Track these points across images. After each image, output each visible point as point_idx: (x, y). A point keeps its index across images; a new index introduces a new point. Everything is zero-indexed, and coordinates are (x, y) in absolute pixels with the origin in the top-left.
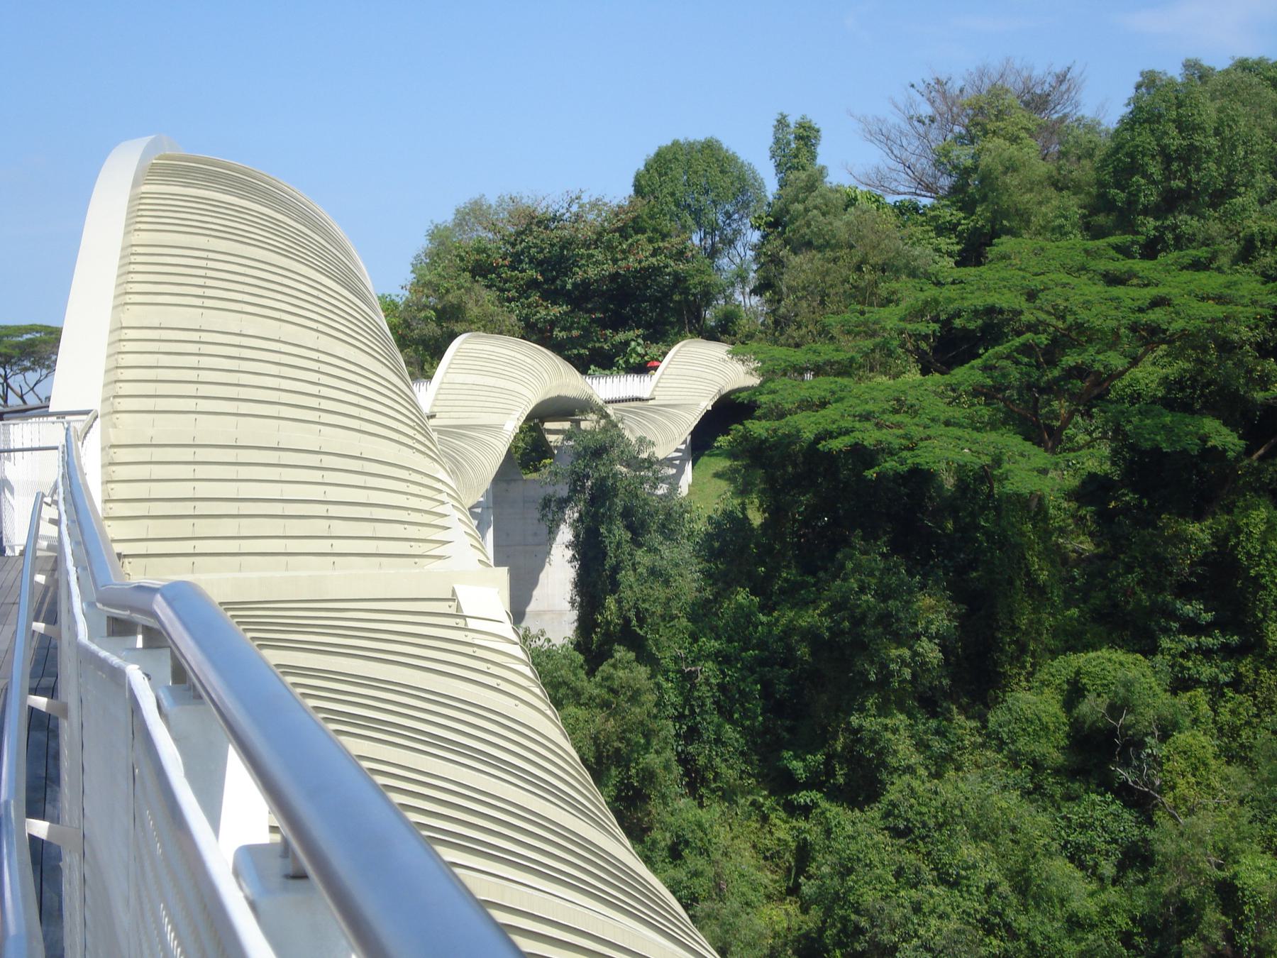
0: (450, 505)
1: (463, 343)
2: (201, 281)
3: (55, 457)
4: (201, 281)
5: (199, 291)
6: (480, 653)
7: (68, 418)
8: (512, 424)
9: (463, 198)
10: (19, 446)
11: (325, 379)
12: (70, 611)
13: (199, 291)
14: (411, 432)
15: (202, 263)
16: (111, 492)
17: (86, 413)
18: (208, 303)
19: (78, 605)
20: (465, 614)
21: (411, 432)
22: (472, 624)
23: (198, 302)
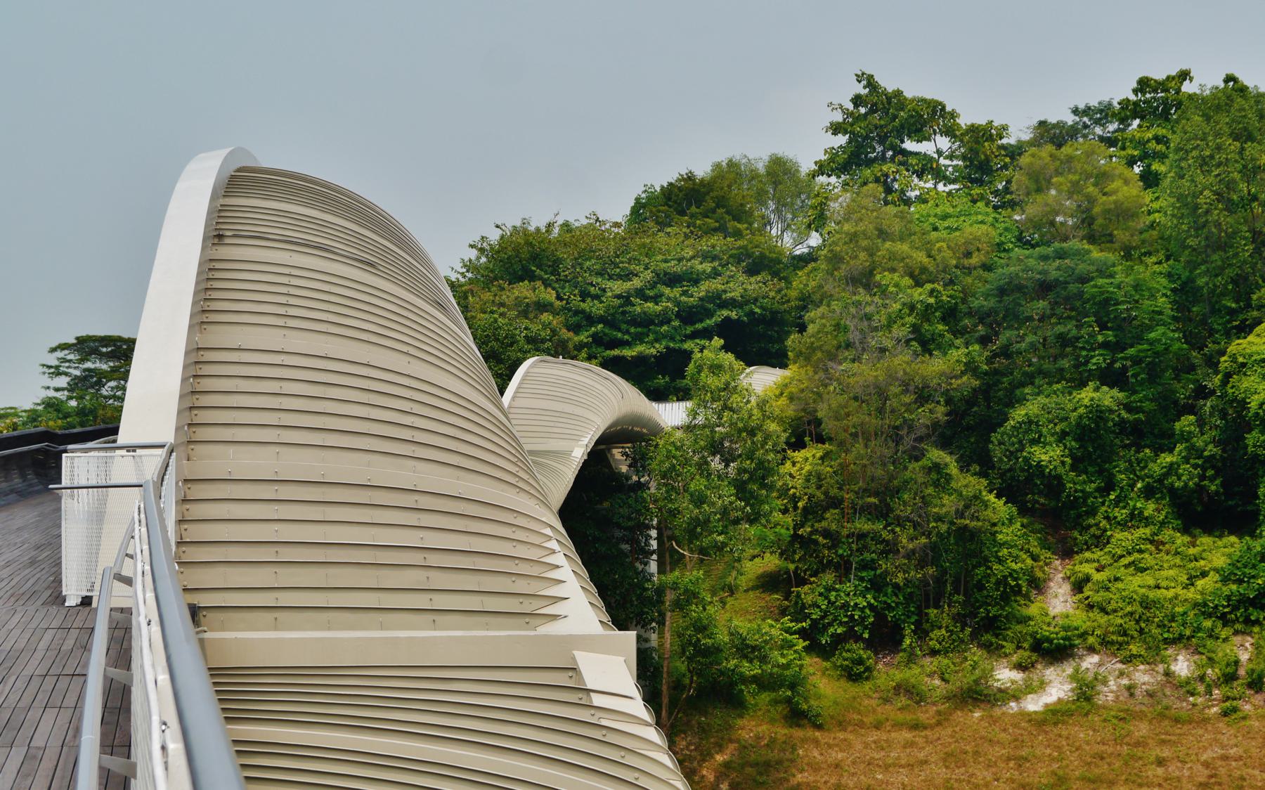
0: (562, 553)
1: (532, 366)
2: (283, 300)
3: (113, 594)
4: (283, 300)
5: (281, 310)
6: (611, 738)
7: (139, 452)
8: (579, 453)
9: (722, 157)
10: (83, 482)
11: (417, 409)
12: (142, 666)
13: (281, 310)
14: (513, 469)
15: (285, 280)
16: (185, 512)
17: (162, 446)
18: (291, 323)
19: (152, 489)
20: (589, 687)
21: (513, 469)
22: (597, 700)
23: (280, 322)
